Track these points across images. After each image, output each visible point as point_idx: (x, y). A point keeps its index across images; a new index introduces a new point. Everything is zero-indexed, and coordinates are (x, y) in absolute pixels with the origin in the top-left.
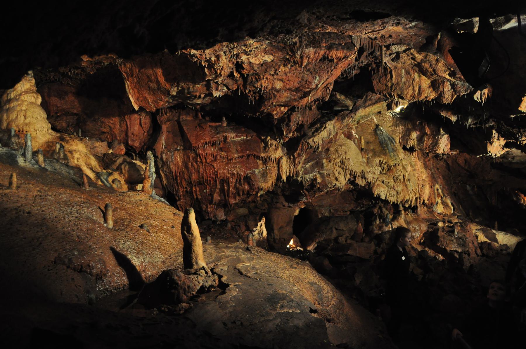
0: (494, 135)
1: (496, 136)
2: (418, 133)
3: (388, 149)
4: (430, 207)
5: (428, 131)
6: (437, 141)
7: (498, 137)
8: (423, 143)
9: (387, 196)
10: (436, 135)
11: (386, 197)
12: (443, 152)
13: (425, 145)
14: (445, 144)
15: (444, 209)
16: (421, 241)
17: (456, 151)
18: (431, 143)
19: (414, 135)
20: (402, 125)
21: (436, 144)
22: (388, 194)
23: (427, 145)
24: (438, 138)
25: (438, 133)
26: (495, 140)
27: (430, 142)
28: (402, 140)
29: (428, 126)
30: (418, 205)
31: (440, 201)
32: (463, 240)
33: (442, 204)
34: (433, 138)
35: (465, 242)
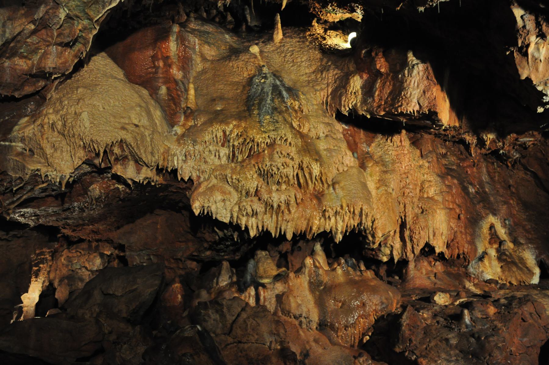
0: (520, 23)
1: (531, 25)
2: (365, 76)
3: (259, 109)
4: (456, 264)
5: (381, 65)
6: (402, 82)
7: (538, 25)
8: (373, 96)
9: (235, 215)
10: (399, 67)
11: (232, 217)
12: (417, 108)
13: (376, 98)
14: (422, 87)
15: (503, 271)
16: (361, 340)
17: (533, 136)
18: (390, 93)
19: (357, 83)
20: (337, 67)
21: (398, 91)
22: (236, 209)
23: (381, 99)
24: (404, 75)
25: (404, 63)
26: (533, 39)
27: (387, 90)
28: (333, 98)
29: (385, 56)
30: (411, 256)
31: (493, 253)
32: (478, 339)
33: (499, 259)
34: (393, 78)
35: (482, 346)
